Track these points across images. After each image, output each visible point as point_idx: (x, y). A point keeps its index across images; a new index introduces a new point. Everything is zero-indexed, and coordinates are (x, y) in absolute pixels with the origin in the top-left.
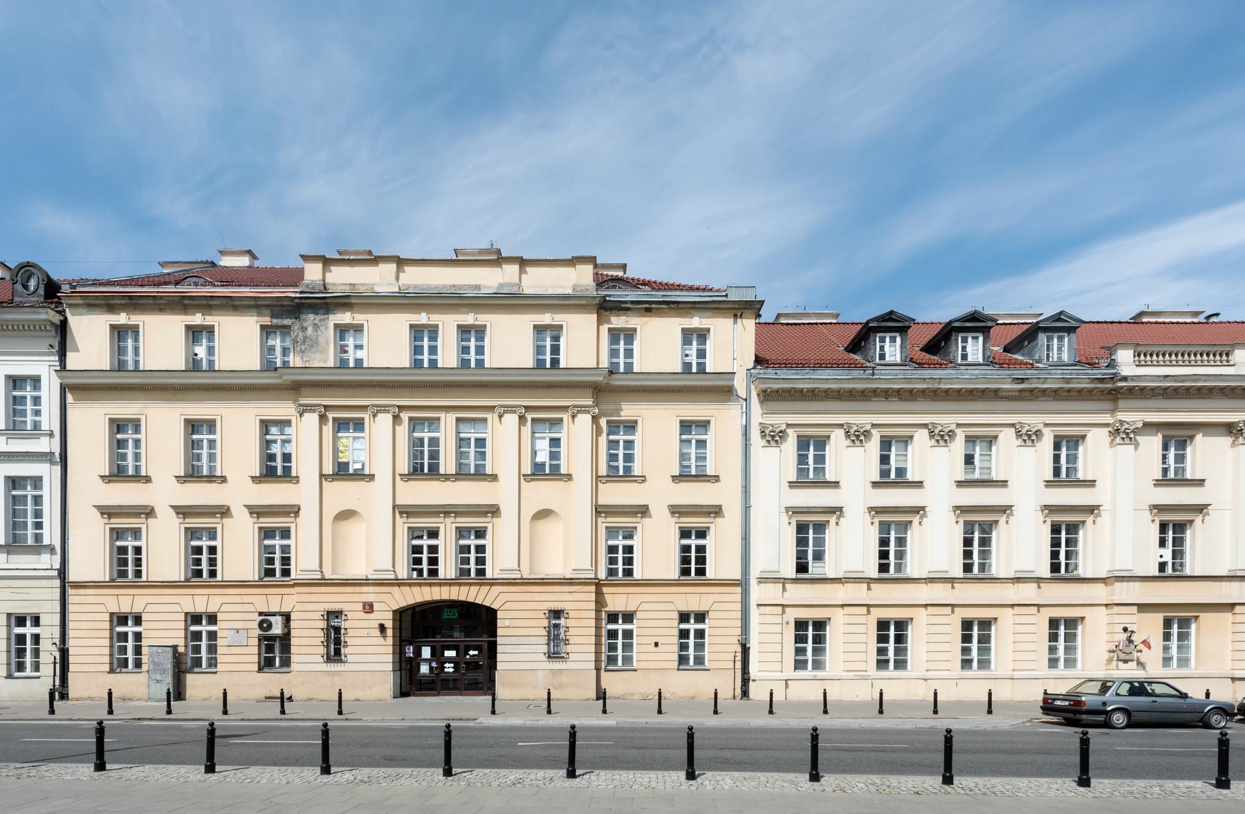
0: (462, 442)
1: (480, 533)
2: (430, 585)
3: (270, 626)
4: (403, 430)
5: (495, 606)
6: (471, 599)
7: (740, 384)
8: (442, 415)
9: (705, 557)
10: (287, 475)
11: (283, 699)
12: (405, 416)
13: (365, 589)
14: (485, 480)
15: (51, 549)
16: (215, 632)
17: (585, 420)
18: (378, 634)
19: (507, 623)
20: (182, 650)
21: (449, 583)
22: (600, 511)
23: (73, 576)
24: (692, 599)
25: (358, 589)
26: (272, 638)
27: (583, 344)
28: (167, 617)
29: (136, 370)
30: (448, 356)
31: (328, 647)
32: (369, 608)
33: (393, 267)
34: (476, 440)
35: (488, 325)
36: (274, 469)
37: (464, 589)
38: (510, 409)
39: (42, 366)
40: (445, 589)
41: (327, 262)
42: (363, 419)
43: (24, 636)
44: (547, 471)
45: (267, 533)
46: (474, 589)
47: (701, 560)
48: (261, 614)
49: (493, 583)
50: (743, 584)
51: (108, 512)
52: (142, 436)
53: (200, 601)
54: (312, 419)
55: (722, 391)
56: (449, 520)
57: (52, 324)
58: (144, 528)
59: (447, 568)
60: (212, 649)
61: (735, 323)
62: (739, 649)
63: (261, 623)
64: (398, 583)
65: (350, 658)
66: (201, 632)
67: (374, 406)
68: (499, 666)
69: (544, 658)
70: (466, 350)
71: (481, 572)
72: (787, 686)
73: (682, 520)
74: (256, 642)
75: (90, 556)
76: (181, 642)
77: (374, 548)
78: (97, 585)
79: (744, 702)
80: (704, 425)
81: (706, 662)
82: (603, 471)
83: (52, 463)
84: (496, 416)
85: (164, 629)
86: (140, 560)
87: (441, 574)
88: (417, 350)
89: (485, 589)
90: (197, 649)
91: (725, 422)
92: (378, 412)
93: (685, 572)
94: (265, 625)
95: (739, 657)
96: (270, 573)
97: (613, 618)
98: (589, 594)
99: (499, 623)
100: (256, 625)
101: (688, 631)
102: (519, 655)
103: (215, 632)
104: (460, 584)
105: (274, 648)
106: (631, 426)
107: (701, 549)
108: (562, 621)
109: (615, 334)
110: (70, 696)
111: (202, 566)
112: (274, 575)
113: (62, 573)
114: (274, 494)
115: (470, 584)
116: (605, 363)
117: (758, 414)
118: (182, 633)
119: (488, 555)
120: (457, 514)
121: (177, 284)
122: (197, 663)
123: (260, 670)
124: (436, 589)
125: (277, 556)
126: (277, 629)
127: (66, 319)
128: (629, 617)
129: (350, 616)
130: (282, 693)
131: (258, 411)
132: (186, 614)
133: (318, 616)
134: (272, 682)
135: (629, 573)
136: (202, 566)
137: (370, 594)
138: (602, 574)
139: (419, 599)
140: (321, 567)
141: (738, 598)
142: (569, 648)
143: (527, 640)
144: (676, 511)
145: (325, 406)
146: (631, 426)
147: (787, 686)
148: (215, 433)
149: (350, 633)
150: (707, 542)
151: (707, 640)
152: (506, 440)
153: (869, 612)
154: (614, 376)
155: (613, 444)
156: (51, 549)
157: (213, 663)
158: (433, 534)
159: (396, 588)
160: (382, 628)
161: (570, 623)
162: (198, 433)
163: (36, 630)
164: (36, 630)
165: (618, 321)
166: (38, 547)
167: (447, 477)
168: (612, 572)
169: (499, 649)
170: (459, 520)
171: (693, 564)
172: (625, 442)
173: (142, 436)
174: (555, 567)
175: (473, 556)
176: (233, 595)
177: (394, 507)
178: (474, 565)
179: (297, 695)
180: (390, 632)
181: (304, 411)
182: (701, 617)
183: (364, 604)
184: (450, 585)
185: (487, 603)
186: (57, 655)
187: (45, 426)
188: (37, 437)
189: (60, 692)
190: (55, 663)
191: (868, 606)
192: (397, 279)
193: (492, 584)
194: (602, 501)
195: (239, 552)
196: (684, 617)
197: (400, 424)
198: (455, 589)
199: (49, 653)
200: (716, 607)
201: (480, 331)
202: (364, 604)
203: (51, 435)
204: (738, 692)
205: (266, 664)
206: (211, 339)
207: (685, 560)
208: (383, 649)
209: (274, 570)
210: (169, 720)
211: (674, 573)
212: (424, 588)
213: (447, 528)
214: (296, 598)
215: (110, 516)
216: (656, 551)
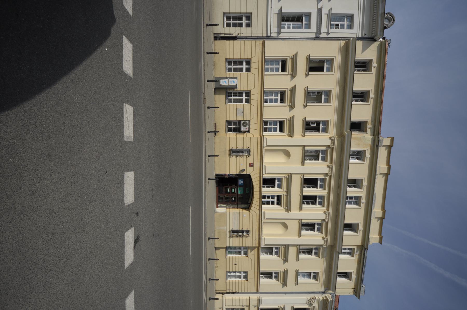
2: (260, 202)
3: (245, 126)
4: (322, 177)
5: (251, 211)
8: (326, 191)
9: (269, 204)
11: (215, 132)
13: (259, 163)
14: (302, 161)
15: (279, 33)
16: (242, 102)
18: (241, 169)
21: (260, 191)
23: (267, 42)
25: (259, 161)
27: (351, 239)
28: (247, 265)
32: (251, 165)
33: (386, 172)
35: (358, 234)
37: (258, 197)
39: (357, 30)
40: (258, 190)
41: (389, 148)
43: (242, 96)
46: (258, 200)
48: (249, 121)
49: (260, 209)
50: (258, 292)
51: (294, 58)
53: (255, 97)
54: (328, 143)
56: (285, 193)
57: (375, 36)
60: (235, 101)
67: (332, 167)
72: (220, 308)
73: (282, 273)
74: (238, 119)
75: (275, 50)
77: (274, 165)
78: (263, 53)
79: (215, 293)
81: (229, 132)
82: (307, 148)
83: (316, 33)
85: (244, 81)
87: (263, 206)
89: (258, 204)
90: (235, 95)
91: (317, 285)
92: (326, 215)
96: (266, 123)
98: (255, 244)
101: (242, 96)
103: (242, 102)
105: (236, 127)
109: (352, 250)
110: (216, 41)
112: (265, 125)
113: (268, 37)
114: (300, 96)
117: (321, 297)
118: (242, 89)
119: (273, 133)
120: (287, 197)
124: (258, 186)
126: (243, 129)
130: (217, 132)
131: (321, 273)
132: (251, 59)
133: (248, 146)
134: (222, 127)
139: (254, 184)
141: (252, 291)
143: (238, 223)
144: (293, 90)
145: (333, 148)
147: (220, 308)
148: (327, 71)
152: (314, 213)
153: (247, 306)
154: (337, 254)
156: (279, 33)
157: (230, 101)
159: (259, 175)
160: (243, 170)
163: (244, 25)
164: (244, 25)
166: (280, 27)
174: (266, 230)
176: (257, 111)
179: (217, 137)
181: (332, 140)
182: (248, 101)
183: (253, 164)
186: (234, 35)
187: (332, 31)
188: (328, 27)
189: (217, 37)
190: (230, 34)
191: (249, 306)
192: (381, 174)
194: (290, 248)
195: (276, 112)
196: (248, 62)
197: (324, 176)
198: (258, 193)
199: (234, 31)
200: (252, 107)
202: (253, 164)
203: (328, 33)
204: (218, 292)
207: (268, 197)
209: (267, 125)
210: (204, 52)
212: (259, 185)
214: (256, 105)
215: (292, 59)
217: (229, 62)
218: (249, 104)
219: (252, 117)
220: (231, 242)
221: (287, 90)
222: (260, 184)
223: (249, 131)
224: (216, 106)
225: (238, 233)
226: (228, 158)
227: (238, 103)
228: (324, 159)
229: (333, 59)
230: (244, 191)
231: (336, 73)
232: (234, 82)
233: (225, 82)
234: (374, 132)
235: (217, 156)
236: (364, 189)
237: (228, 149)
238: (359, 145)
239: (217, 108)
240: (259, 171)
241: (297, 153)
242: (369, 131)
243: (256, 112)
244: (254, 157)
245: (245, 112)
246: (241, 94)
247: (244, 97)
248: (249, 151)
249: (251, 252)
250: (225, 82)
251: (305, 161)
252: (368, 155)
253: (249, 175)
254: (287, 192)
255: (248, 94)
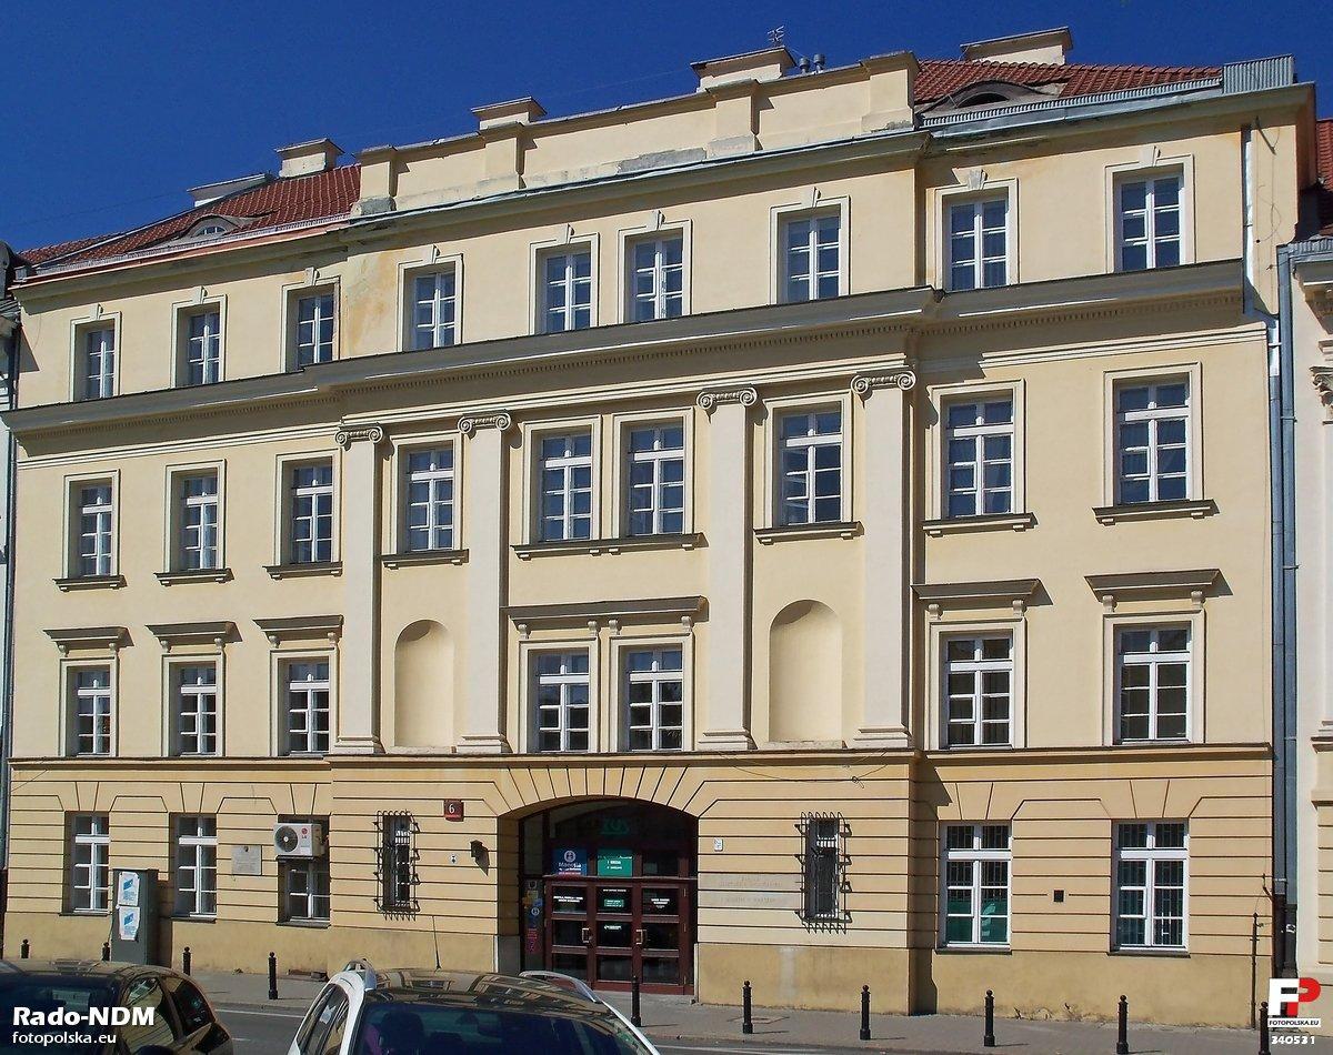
0: (635, 474)
1: (671, 656)
2: (666, 764)
3: (293, 843)
5: (693, 810)
6: (645, 795)
7: (1261, 277)
8: (594, 422)
10: (326, 564)
12: (527, 429)
17: (889, 402)
18: (473, 861)
19: (718, 844)
20: (164, 877)
21: (604, 762)
22: (920, 597)
24: (1146, 792)
25: (436, 773)
26: (301, 862)
29: (215, 383)
30: (608, 306)
31: (386, 883)
32: (455, 810)
34: (1006, 439)
36: (305, 549)
37: (633, 774)
38: (725, 396)
42: (450, 444)
44: (979, 511)
45: (1130, 638)
46: (652, 774)
47: (1173, 699)
48: (283, 818)
51: (68, 639)
52: (333, 489)
55: (1222, 299)
56: (606, 632)
58: (687, 643)
59: (605, 733)
61: (1245, 139)
62: (1266, 907)
63: (280, 835)
64: (506, 761)
65: (424, 907)
66: (969, 864)
67: (864, 375)
68: (703, 934)
69: (373, 906)
70: (1132, 227)
71: (671, 740)
74: (274, 868)
76: (162, 866)
77: (463, 695)
80: (1173, 390)
84: (701, 411)
85: (139, 845)
86: (326, 715)
88: (1132, 227)
91: (1226, 373)
92: (872, 387)
93: (1129, 726)
94: (286, 840)
95: (1267, 929)
97: (960, 834)
99: (703, 845)
100: (271, 838)
102: (743, 917)
104: (625, 765)
105: (304, 883)
106: (999, 408)
107: (1173, 676)
108: (837, 842)
109: (958, 213)
110: (940, 1004)
111: (191, 730)
112: (970, 740)
115: (645, 764)
116: (936, 278)
118: (164, 850)
119: (1015, 694)
120: (623, 621)
121: (183, 235)
122: (961, 930)
123: (283, 919)
125: (562, 709)
126: (305, 849)
127: (20, 326)
128: (996, 834)
129: (424, 825)
132: (172, 815)
133: (368, 824)
135: (996, 734)
136: (191, 730)
137: (454, 784)
138: (932, 740)
140: (747, 724)
142: (851, 901)
144: (1109, 587)
145: (757, 387)
146: (999, 408)
149: (425, 858)
150: (1013, 664)
151: (1186, 887)
152: (721, 456)
155: (956, 450)
158: (578, 661)
159: (505, 771)
160: (478, 851)
161: (852, 846)
162: (420, 469)
163: (103, 840)
164: (103, 840)
165: (968, 179)
167: (603, 546)
168: (957, 735)
169: (702, 898)
170: (627, 630)
171: (1147, 708)
172: (1162, 424)
173: (333, 489)
174: (825, 725)
175: (654, 705)
177: (506, 612)
178: (654, 719)
180: (493, 859)
182: (1171, 833)
183: (447, 802)
184: (605, 765)
185: (677, 804)
193: (687, 764)
196: (1129, 833)
198: (614, 774)
201: (672, 245)
205: (290, 911)
206: (449, 289)
208: (480, 893)
209: (305, 737)
211: (1097, 729)
213: (603, 648)
214: (223, 790)
215: (1118, 597)
216: (1061, 681)
217: (1125, 934)
218: (1016, 829)
219: (264, 807)
220: (878, 913)
221: (276, 656)
222: (548, 765)
223: (322, 823)
224: (1115, 1013)
225: (823, 882)
226: (420, 922)
227: (1186, 888)
228: (829, 420)
229: (1116, 383)
230: (616, 846)
231: (1183, 357)
232: (127, 885)
233: (128, 920)
234: (332, 250)
235: (747, 991)
236: (585, 229)
237: (380, 920)
238: (381, 309)
239: (1123, 1006)
240: (485, 774)
241: (794, 567)
242: (328, 273)
243: (245, 791)
244: (418, 796)
245: (247, 838)
246: (183, 855)
247: (1150, 854)
248: (825, 826)
249: (946, 801)
250: (128, 920)
251: (1189, 496)
252: (422, 255)
253: (503, 820)
254: (602, 622)
255: (184, 823)
